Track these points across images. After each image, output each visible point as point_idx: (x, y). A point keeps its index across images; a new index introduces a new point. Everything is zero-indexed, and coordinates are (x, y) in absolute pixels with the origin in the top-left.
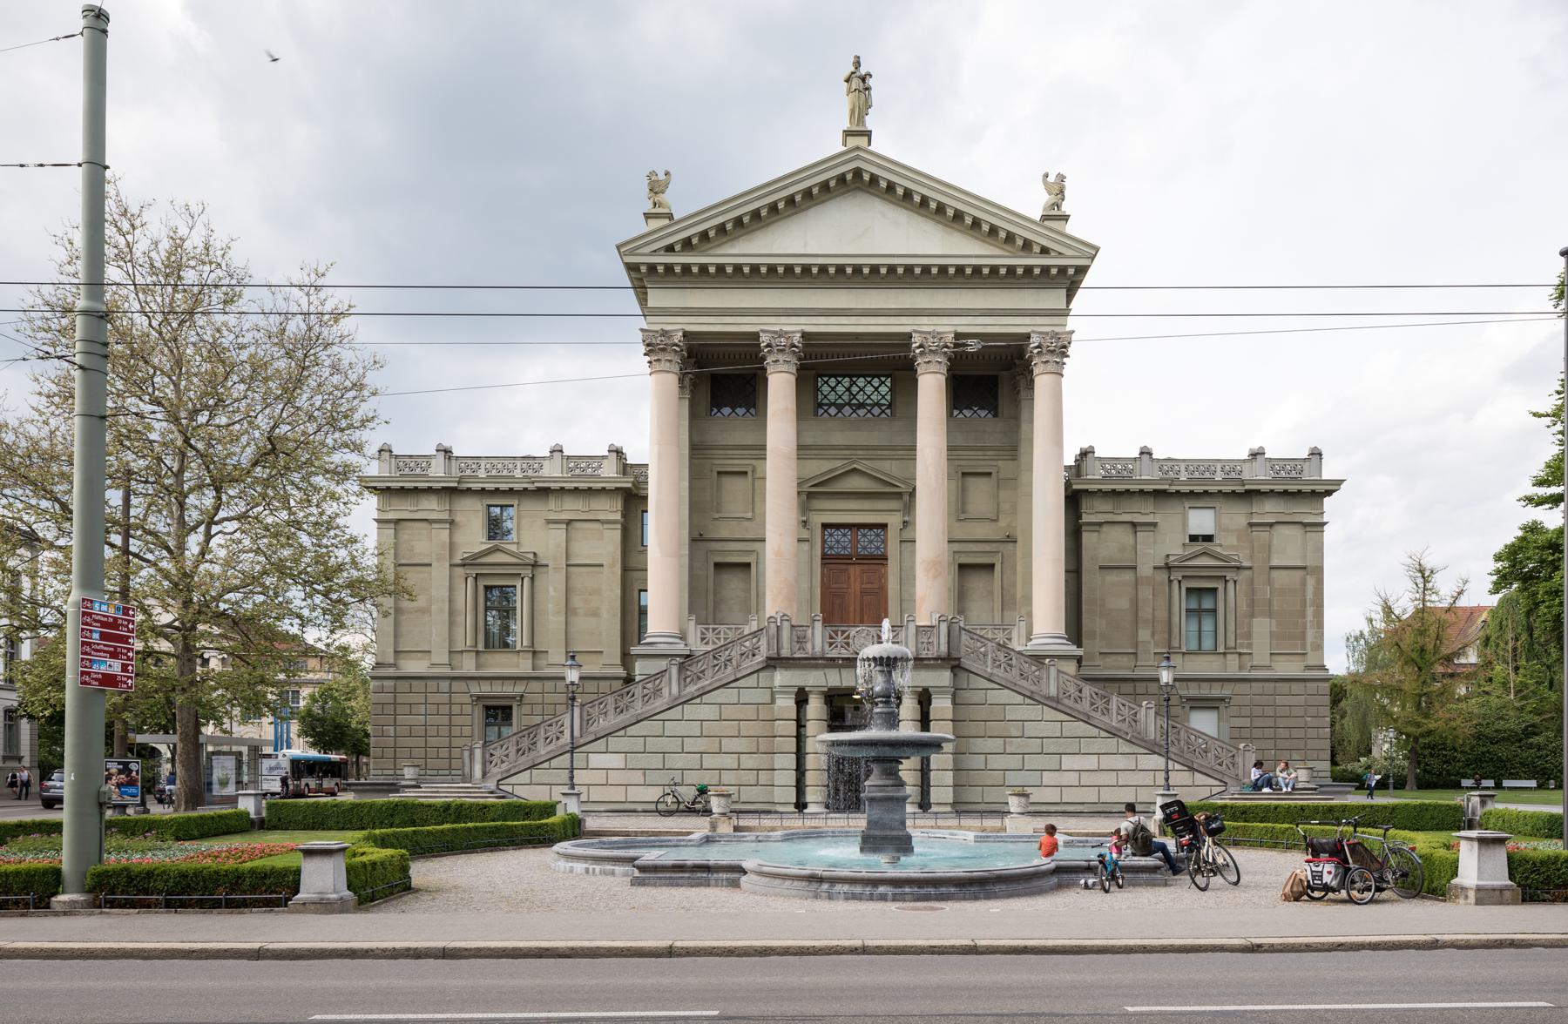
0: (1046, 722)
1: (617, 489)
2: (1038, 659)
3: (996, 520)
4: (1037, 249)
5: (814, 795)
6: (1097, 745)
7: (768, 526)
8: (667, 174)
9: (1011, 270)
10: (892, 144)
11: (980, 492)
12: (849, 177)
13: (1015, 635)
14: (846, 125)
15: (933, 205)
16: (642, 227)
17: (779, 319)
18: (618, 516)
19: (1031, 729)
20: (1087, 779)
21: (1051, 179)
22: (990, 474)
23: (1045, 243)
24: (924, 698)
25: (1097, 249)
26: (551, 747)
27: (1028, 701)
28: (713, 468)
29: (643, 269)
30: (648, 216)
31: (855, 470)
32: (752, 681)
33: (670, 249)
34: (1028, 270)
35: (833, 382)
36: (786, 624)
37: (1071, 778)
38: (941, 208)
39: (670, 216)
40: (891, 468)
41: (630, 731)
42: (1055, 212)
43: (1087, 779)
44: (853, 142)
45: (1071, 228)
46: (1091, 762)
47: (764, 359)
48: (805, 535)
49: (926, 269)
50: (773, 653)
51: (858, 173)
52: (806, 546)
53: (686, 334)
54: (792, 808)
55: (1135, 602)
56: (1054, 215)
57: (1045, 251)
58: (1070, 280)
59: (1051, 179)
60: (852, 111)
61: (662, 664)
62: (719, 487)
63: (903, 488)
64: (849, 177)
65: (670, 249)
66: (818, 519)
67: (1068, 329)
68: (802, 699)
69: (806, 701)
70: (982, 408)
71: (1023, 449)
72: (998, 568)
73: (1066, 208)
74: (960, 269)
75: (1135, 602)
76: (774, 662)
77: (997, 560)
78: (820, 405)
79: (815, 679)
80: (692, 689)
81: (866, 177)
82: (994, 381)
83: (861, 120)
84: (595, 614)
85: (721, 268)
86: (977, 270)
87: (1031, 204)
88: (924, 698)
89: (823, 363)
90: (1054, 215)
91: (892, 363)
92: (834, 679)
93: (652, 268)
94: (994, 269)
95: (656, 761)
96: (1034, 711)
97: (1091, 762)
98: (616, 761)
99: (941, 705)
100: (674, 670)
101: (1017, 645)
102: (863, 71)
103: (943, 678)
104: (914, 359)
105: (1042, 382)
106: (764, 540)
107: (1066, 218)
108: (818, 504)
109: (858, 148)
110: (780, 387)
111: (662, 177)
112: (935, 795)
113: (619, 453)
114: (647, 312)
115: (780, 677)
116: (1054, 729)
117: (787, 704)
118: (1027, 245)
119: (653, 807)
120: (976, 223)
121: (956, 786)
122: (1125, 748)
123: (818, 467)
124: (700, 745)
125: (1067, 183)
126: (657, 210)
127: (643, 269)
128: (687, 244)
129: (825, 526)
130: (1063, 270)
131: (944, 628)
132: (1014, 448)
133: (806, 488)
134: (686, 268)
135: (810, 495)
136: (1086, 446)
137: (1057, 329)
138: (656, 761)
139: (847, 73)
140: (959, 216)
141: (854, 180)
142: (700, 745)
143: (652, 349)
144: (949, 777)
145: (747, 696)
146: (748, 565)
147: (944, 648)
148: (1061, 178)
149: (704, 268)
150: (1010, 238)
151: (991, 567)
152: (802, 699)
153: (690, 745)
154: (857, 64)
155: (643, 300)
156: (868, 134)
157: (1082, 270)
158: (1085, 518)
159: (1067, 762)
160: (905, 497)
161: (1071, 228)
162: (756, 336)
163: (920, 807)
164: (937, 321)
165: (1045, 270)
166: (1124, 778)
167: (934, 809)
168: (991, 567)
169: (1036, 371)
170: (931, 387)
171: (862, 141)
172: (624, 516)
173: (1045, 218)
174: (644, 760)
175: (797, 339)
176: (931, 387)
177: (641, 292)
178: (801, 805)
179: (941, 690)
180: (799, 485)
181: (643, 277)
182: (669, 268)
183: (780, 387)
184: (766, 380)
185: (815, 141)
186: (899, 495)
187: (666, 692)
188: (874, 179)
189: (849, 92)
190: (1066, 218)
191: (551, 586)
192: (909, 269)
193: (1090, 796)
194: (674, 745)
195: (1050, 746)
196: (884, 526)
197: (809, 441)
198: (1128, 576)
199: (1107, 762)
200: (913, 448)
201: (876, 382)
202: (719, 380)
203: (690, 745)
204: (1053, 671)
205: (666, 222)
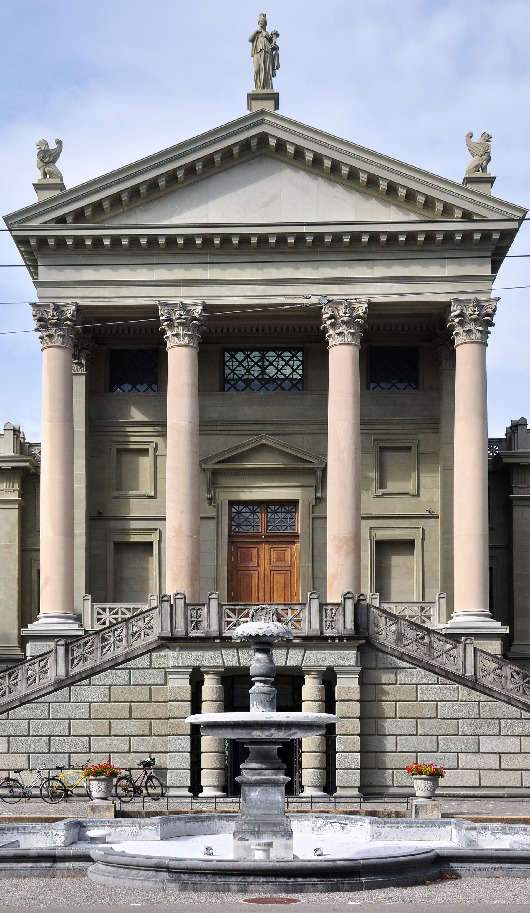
0: (458, 702)
1: (14, 468)
2: (454, 637)
3: (418, 495)
4: (458, 214)
5: (208, 778)
6: (517, 727)
7: (168, 504)
8: (59, 143)
9: (430, 236)
10: (310, 105)
12: (254, 143)
13: (434, 612)
14: (251, 88)
15: (345, 170)
16: (32, 198)
17: (179, 291)
18: (15, 496)
19: (444, 709)
20: (507, 762)
21: (476, 139)
22: (409, 448)
23: (468, 206)
24: (329, 679)
25: (525, 212)
27: (441, 680)
29: (33, 243)
30: (38, 187)
31: (264, 445)
32: (144, 661)
34: (449, 235)
35: (240, 356)
36: (180, 604)
37: (492, 761)
38: (353, 174)
39: (61, 187)
40: (300, 444)
42: (480, 174)
43: (507, 762)
44: (258, 105)
45: (496, 191)
46: (513, 744)
47: (164, 332)
48: (211, 511)
49: (226, 239)
50: (167, 634)
51: (263, 138)
52: (212, 524)
53: (206, 308)
54: (186, 792)
56: (478, 178)
57: (467, 216)
58: (495, 247)
59: (476, 139)
60: (258, 73)
61: (50, 645)
62: (119, 464)
63: (316, 463)
64: (254, 143)
65: (61, 220)
66: (225, 496)
67: (494, 295)
68: (197, 679)
69: (202, 682)
70: (401, 381)
71: (443, 423)
73: (492, 170)
74: (374, 237)
76: (169, 642)
77: (417, 536)
78: (226, 380)
79: (208, 659)
81: (272, 142)
82: (410, 355)
83: (267, 83)
85: (116, 240)
86: (393, 237)
87: (453, 165)
88: (329, 679)
89: (222, 337)
90: (478, 178)
91: (300, 334)
92: (230, 658)
93: (42, 241)
94: (411, 236)
95: (42, 744)
97: (513, 744)
99: (347, 686)
100: (61, 651)
101: (435, 624)
102: (270, 30)
103: (348, 657)
104: (325, 330)
105: (464, 354)
106: (164, 519)
107: (491, 180)
108: (224, 481)
109: (262, 112)
110: (180, 362)
111: (53, 146)
112: (340, 778)
113: (16, 432)
114: (38, 284)
115: (171, 657)
117: (181, 685)
118: (448, 209)
120: (392, 188)
121: (363, 769)
123: (222, 444)
124: (90, 727)
125: (493, 144)
126: (49, 181)
127: (33, 243)
128: (79, 216)
129: (232, 503)
130: (486, 235)
131: (350, 605)
132: (437, 421)
133: (211, 465)
134: (79, 241)
135: (216, 473)
136: (517, 418)
137: (480, 297)
138: (42, 744)
139: (251, 33)
140: (373, 182)
142: (90, 727)
143: (43, 323)
144: (355, 743)
145: (137, 677)
146: (150, 544)
147: (350, 626)
148: (488, 138)
149: (98, 241)
150: (429, 202)
151: (411, 544)
152: (197, 679)
153: (77, 727)
154: (264, 25)
155: (34, 274)
157: (509, 236)
158: (517, 493)
159: (486, 744)
160: (315, 474)
161: (496, 191)
162: (153, 310)
164: (354, 289)
165: (468, 235)
167: (339, 792)
168: (411, 544)
169: (457, 341)
170: (342, 360)
171: (268, 106)
172: (21, 495)
173: (468, 180)
174: (28, 744)
175: (197, 311)
176: (342, 360)
177: (33, 266)
178: (196, 788)
179: (347, 670)
180: (201, 463)
181: (35, 251)
182: (61, 241)
183: (180, 362)
184: (167, 353)
185: (216, 106)
186: (311, 471)
188: (281, 144)
189: (254, 52)
190: (491, 180)
192: (282, 238)
193: (511, 779)
194: (61, 727)
197: (214, 414)
200: (325, 423)
201: (287, 355)
202: (114, 357)
203: (77, 727)
204: (470, 649)
205: (57, 193)
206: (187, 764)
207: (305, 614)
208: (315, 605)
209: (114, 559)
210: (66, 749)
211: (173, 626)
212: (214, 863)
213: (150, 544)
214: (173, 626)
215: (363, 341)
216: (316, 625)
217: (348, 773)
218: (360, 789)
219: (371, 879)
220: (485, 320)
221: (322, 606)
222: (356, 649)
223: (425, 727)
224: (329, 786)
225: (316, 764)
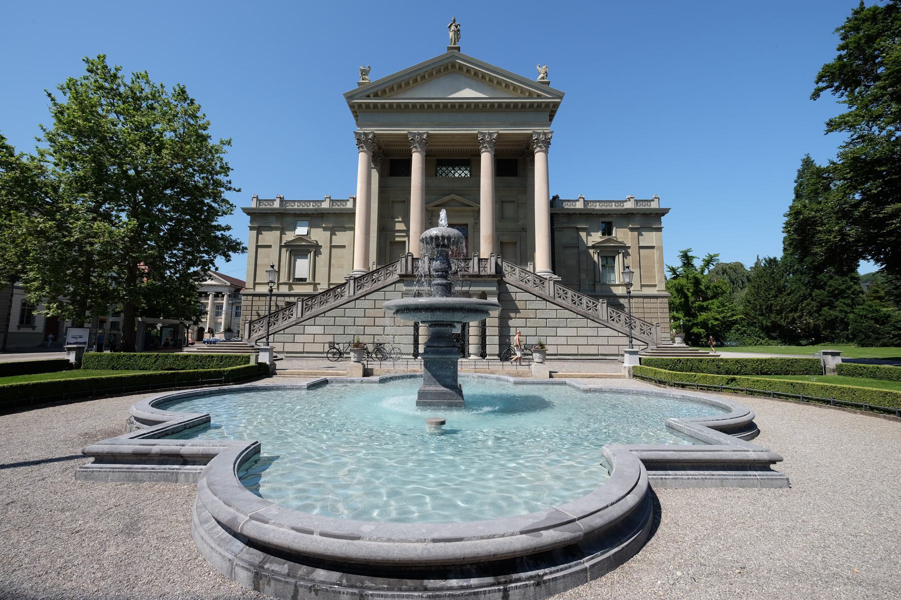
0: (551, 311)
6: (576, 323)
10: (473, 50)
11: (509, 210)
19: (540, 314)
26: (286, 322)
28: (391, 204)
32: (392, 288)
33: (368, 97)
37: (563, 341)
41: (327, 314)
46: (573, 332)
50: (404, 272)
55: (579, 262)
58: (550, 111)
72: (518, 243)
75: (579, 262)
80: (359, 293)
82: (514, 165)
84: (341, 267)
93: (360, 105)
96: (541, 304)
98: (319, 330)
112: (489, 350)
116: (553, 314)
119: (325, 355)
122: (591, 324)
141: (450, 67)
144: (496, 331)
146: (405, 242)
153: (359, 321)
156: (458, 49)
159: (560, 331)
163: (481, 356)
166: (591, 341)
167: (488, 357)
174: (334, 330)
181: (358, 110)
185: (435, 50)
187: (347, 294)
191: (526, 369)
193: (593, 350)
194: (350, 321)
195: (551, 323)
196: (467, 225)
198: (575, 251)
199: (582, 332)
202: (390, 163)
203: (359, 321)
206: (412, 341)
207: (471, 264)
208: (476, 259)
209: (389, 247)
210: (353, 332)
211: (406, 270)
212: (316, 537)
213: (405, 242)
214: (406, 270)
215: (495, 156)
216: (476, 269)
217: (493, 347)
218: (499, 355)
219: (600, 557)
220: (547, 143)
221: (480, 260)
222: (496, 284)
223: (530, 323)
224: (483, 355)
225: (476, 342)
